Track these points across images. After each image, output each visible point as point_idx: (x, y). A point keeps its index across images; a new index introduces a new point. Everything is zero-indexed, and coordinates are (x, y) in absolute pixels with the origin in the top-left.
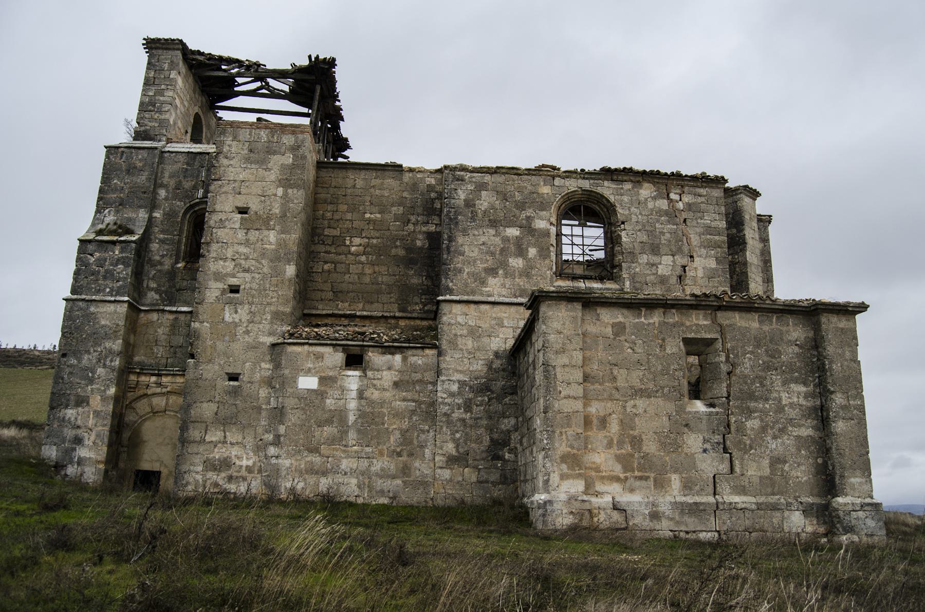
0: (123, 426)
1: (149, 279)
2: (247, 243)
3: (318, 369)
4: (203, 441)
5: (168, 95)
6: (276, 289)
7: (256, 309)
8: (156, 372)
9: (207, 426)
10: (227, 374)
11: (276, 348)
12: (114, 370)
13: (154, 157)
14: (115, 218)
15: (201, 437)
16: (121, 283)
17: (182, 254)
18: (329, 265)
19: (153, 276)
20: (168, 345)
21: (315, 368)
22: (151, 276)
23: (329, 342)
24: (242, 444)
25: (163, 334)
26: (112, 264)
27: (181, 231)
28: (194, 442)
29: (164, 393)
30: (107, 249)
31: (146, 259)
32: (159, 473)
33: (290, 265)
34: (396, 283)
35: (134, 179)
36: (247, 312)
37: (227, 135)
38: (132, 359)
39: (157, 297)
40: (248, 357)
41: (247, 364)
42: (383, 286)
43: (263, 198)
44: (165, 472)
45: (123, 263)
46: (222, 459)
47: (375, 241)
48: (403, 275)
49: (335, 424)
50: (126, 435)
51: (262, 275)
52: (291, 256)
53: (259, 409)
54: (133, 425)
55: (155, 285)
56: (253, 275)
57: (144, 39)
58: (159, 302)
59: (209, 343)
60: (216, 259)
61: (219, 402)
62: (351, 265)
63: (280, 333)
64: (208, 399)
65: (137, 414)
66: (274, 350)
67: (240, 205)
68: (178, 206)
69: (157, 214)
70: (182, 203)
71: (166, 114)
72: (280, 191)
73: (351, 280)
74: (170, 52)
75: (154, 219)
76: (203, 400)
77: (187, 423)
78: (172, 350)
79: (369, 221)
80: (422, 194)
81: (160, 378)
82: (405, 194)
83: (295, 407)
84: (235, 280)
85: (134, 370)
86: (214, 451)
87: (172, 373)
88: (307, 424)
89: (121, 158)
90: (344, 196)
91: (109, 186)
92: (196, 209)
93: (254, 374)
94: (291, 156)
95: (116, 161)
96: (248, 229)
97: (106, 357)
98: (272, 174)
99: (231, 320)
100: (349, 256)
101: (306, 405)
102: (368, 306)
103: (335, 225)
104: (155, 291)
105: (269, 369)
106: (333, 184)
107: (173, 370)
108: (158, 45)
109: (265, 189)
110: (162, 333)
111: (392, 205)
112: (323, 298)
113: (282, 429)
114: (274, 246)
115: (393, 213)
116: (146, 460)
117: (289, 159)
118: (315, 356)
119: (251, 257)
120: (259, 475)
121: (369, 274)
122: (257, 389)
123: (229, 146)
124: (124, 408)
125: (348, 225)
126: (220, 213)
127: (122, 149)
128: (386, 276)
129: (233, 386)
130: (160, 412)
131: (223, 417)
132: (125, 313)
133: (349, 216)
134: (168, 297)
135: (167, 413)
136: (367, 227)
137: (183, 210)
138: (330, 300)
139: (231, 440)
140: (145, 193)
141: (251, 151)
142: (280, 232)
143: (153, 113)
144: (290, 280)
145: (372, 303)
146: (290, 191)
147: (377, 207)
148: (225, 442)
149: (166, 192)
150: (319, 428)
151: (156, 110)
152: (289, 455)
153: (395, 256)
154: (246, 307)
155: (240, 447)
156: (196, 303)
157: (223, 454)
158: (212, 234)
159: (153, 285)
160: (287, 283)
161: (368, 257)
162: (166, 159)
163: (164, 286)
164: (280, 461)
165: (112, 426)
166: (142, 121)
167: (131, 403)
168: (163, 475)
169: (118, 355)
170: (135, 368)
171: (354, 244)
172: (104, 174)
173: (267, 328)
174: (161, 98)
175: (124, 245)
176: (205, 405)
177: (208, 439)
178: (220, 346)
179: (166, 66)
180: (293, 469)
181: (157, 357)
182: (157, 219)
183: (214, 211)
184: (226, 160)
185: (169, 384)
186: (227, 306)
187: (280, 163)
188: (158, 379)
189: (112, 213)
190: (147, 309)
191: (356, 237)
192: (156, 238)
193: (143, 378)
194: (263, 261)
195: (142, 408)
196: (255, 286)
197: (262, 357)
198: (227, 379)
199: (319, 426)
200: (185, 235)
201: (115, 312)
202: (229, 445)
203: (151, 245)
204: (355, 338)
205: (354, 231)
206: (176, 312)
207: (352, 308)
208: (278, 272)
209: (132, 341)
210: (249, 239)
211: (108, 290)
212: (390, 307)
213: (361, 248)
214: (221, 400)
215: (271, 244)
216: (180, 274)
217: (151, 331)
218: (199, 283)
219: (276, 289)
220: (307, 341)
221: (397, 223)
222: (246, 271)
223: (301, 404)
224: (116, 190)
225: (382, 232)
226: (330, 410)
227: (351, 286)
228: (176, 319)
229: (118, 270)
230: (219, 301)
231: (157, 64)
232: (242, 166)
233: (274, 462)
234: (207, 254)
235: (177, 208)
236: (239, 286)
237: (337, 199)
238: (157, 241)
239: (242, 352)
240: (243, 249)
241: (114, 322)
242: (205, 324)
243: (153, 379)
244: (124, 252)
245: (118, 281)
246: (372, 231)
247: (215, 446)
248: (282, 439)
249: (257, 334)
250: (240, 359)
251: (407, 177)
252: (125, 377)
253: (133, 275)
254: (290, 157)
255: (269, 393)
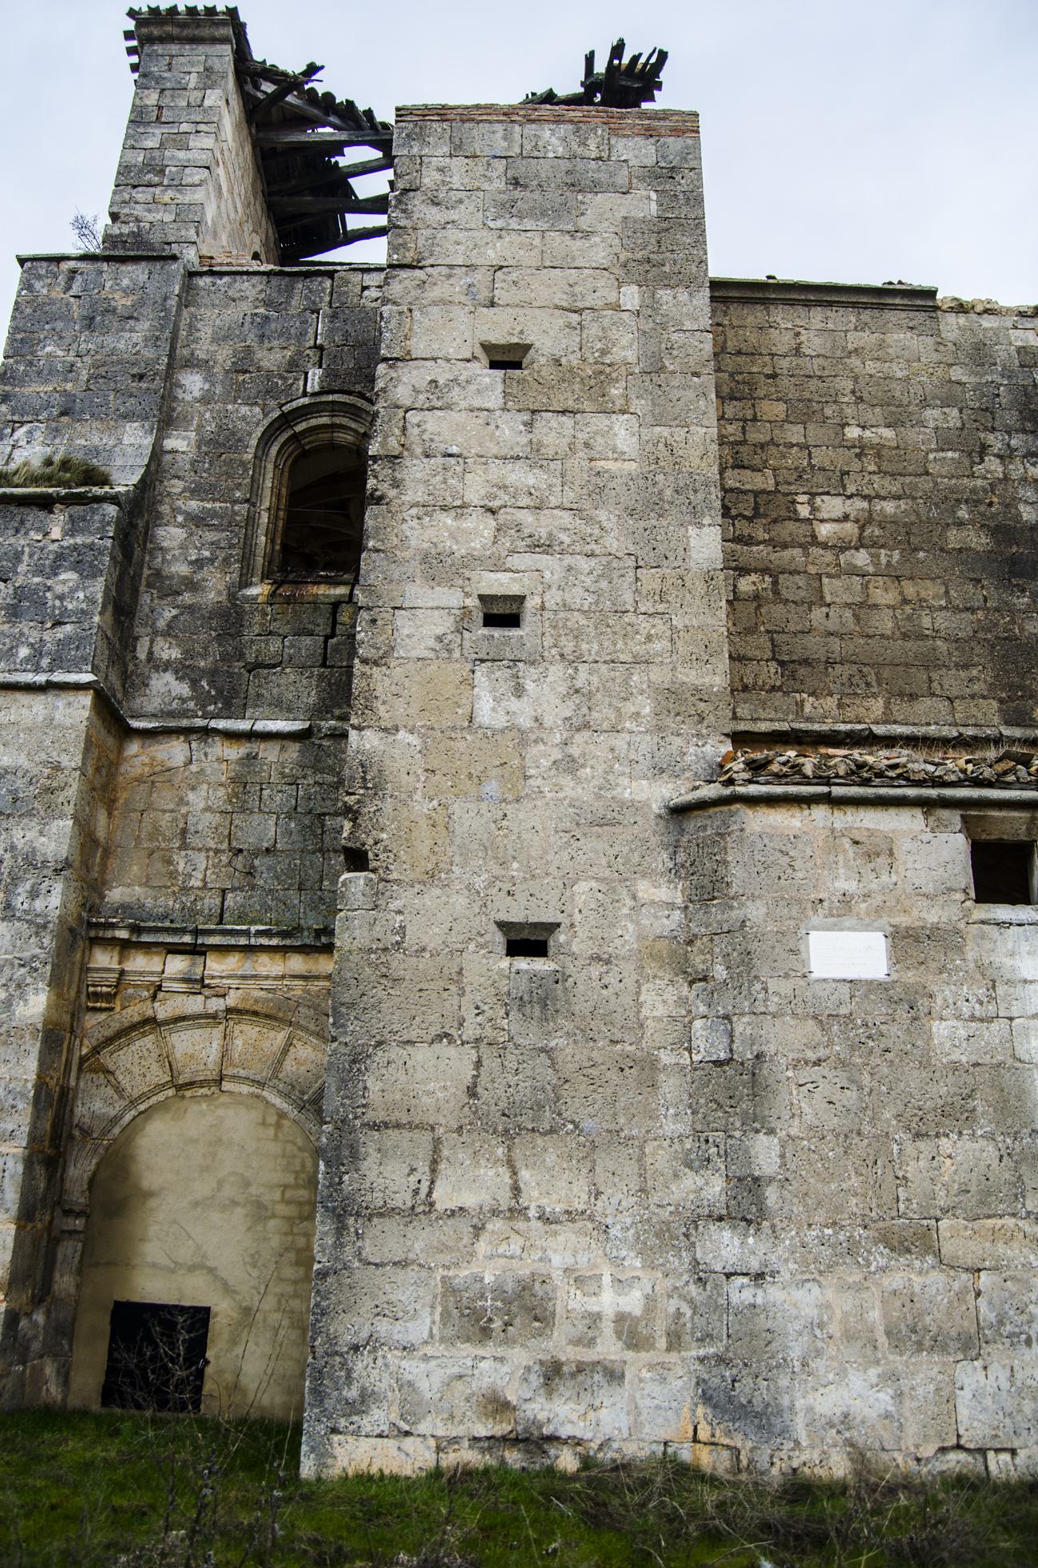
0: (71, 1137)
1: (155, 633)
2: (534, 456)
3: (880, 898)
4: (422, 1209)
5: (199, 145)
6: (661, 608)
7: (595, 679)
8: (187, 939)
9: (437, 1143)
10: (502, 925)
11: (692, 824)
12: (44, 927)
13: (168, 282)
14: (49, 449)
15: (416, 1192)
16: (68, 628)
17: (260, 560)
18: (753, 577)
19: (169, 626)
20: (225, 846)
21: (867, 896)
22: (161, 624)
23: (912, 792)
24: (591, 1218)
25: (208, 809)
26: (39, 571)
27: (255, 487)
28: (386, 1212)
29: (214, 1016)
30: (22, 522)
31: (146, 572)
32: (200, 1317)
33: (700, 525)
34: (981, 635)
35: (109, 341)
36: (563, 690)
37: (431, 140)
38: (102, 897)
39: (183, 689)
40: (581, 859)
41: (582, 887)
42: (939, 643)
43: (575, 317)
44: (223, 1311)
45: (77, 566)
46: (510, 1287)
47: (889, 507)
48: (997, 610)
49: (984, 1127)
50: (80, 1169)
51: (604, 560)
52: (700, 496)
53: (649, 1066)
54: (105, 1132)
55: (175, 654)
56: (568, 560)
57: (132, 13)
58: (191, 705)
59: (421, 806)
60: (428, 508)
61: (477, 1040)
62: (825, 580)
63: (700, 767)
64: (435, 1030)
65: (119, 1090)
66: (682, 832)
67: (498, 337)
68: (244, 418)
69: (179, 442)
70: (257, 410)
71: (194, 193)
72: (631, 296)
73: (832, 625)
74: (202, 49)
75: (168, 457)
76: (413, 1036)
77: (353, 1130)
78: (239, 863)
79: (861, 449)
80: (1007, 373)
81: (200, 960)
82: (957, 373)
83: (811, 1055)
84: (504, 577)
85: (109, 934)
86: (472, 1254)
87: (243, 941)
88: (866, 1129)
89: (68, 288)
90: (768, 376)
91: (31, 363)
92: (299, 428)
93: (612, 925)
94: (654, 196)
95: (53, 295)
96: (533, 412)
97: (15, 880)
98: (596, 245)
99: (501, 721)
100: (815, 551)
101: (852, 1048)
102: (900, 709)
103: (757, 461)
104: (176, 672)
105: (671, 906)
106: (729, 343)
107: (247, 933)
108: (168, 29)
109: (577, 289)
110: (202, 805)
111: (924, 403)
112: (748, 680)
113: (765, 1154)
114: (633, 465)
115: (932, 424)
116: (154, 1265)
117: (646, 204)
118: (860, 849)
119: (554, 502)
120: (673, 1357)
121: (888, 607)
122: (632, 988)
123: (441, 170)
124: (75, 1068)
125: (796, 458)
126: (429, 364)
127: (72, 264)
128: (943, 614)
129: (533, 976)
130: (202, 1084)
131: (503, 1104)
132: (82, 727)
133: (795, 434)
134: (220, 692)
135: (226, 1086)
136: (856, 465)
137: (261, 429)
138: (773, 689)
139: (544, 1201)
140: (141, 377)
141: (516, 183)
142: (649, 419)
143: (158, 190)
144: (709, 579)
145: (913, 697)
146: (664, 295)
147: (878, 410)
148: (517, 1212)
149: (206, 380)
150: (922, 1145)
151: (166, 182)
152: (814, 1271)
153: (960, 550)
154: (557, 672)
155: (582, 1232)
156: (365, 661)
157: (515, 1263)
158: (404, 429)
159: (168, 651)
160: (700, 587)
161: (878, 556)
162: (202, 293)
163: (204, 656)
164: (773, 1294)
165: (33, 1138)
166: (126, 211)
167: (96, 1051)
168: (219, 1325)
169: (57, 871)
170: (113, 926)
171: (824, 515)
172: (14, 330)
173: (644, 748)
174: (181, 155)
175: (77, 510)
176: (422, 1054)
177: (445, 1197)
178: (469, 818)
179: (193, 80)
180: (834, 1328)
181: (185, 890)
182: (179, 457)
183: (406, 358)
184: (434, 210)
185: (234, 983)
186: (481, 670)
187: (619, 216)
188: (193, 965)
189: (38, 435)
190: (150, 726)
191: (828, 493)
192: (175, 511)
193: (139, 963)
194: (602, 515)
195: (136, 1070)
196: (577, 596)
197: (636, 858)
198: (502, 949)
199: (918, 1135)
200: (266, 504)
201: (50, 721)
202: (536, 1224)
203: (160, 532)
204: (1005, 773)
205: (820, 478)
206: (251, 736)
207: (850, 713)
208: (662, 548)
209: (101, 834)
210: (540, 444)
211: (24, 652)
212: (974, 711)
213: (850, 528)
214: (489, 1032)
215: (620, 457)
216: (258, 618)
217: (164, 799)
218: (370, 589)
219: (661, 608)
220: (825, 789)
221: (950, 454)
222: (538, 546)
223: (830, 1044)
224: (52, 371)
225: (908, 480)
226: (955, 1067)
227: (835, 644)
228: (251, 758)
229: (59, 589)
230: (450, 651)
231: (165, 75)
232: (492, 224)
233: (747, 1296)
234: (392, 493)
235: (240, 425)
236: (520, 599)
237: (752, 385)
238: (180, 519)
239: (558, 840)
240: (521, 476)
241: (44, 756)
242: (402, 735)
243: (177, 965)
244: (82, 531)
245: (58, 623)
246: (875, 478)
247: (478, 1230)
248: (771, 1195)
249: (610, 770)
250: (552, 869)
251: (951, 325)
252: (78, 956)
253: (110, 608)
254: (649, 198)
255: (682, 1001)
